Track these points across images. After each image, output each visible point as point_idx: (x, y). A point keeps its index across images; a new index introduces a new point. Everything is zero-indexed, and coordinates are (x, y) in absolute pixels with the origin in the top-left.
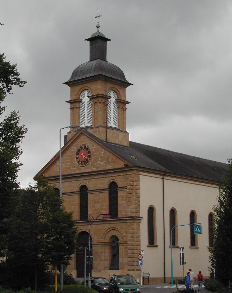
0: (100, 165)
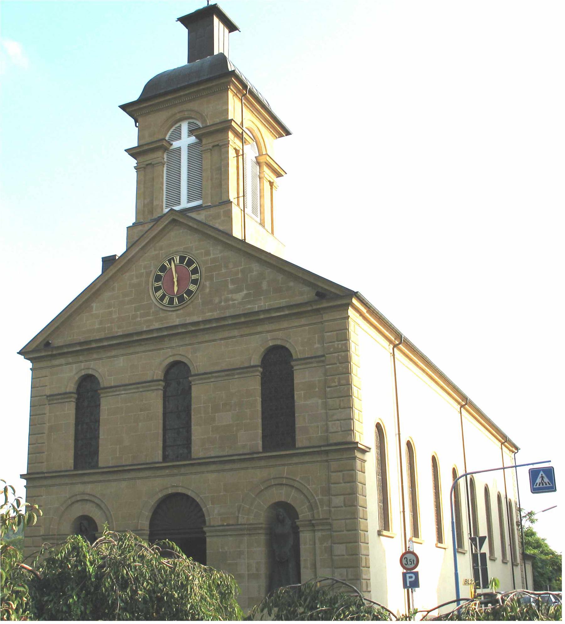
0: (231, 302)
